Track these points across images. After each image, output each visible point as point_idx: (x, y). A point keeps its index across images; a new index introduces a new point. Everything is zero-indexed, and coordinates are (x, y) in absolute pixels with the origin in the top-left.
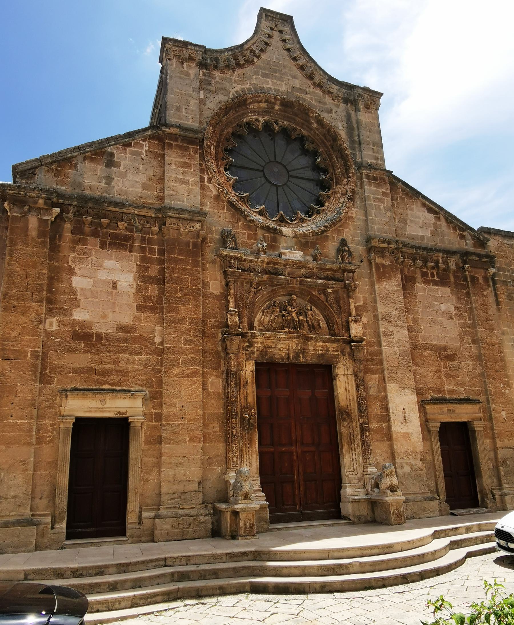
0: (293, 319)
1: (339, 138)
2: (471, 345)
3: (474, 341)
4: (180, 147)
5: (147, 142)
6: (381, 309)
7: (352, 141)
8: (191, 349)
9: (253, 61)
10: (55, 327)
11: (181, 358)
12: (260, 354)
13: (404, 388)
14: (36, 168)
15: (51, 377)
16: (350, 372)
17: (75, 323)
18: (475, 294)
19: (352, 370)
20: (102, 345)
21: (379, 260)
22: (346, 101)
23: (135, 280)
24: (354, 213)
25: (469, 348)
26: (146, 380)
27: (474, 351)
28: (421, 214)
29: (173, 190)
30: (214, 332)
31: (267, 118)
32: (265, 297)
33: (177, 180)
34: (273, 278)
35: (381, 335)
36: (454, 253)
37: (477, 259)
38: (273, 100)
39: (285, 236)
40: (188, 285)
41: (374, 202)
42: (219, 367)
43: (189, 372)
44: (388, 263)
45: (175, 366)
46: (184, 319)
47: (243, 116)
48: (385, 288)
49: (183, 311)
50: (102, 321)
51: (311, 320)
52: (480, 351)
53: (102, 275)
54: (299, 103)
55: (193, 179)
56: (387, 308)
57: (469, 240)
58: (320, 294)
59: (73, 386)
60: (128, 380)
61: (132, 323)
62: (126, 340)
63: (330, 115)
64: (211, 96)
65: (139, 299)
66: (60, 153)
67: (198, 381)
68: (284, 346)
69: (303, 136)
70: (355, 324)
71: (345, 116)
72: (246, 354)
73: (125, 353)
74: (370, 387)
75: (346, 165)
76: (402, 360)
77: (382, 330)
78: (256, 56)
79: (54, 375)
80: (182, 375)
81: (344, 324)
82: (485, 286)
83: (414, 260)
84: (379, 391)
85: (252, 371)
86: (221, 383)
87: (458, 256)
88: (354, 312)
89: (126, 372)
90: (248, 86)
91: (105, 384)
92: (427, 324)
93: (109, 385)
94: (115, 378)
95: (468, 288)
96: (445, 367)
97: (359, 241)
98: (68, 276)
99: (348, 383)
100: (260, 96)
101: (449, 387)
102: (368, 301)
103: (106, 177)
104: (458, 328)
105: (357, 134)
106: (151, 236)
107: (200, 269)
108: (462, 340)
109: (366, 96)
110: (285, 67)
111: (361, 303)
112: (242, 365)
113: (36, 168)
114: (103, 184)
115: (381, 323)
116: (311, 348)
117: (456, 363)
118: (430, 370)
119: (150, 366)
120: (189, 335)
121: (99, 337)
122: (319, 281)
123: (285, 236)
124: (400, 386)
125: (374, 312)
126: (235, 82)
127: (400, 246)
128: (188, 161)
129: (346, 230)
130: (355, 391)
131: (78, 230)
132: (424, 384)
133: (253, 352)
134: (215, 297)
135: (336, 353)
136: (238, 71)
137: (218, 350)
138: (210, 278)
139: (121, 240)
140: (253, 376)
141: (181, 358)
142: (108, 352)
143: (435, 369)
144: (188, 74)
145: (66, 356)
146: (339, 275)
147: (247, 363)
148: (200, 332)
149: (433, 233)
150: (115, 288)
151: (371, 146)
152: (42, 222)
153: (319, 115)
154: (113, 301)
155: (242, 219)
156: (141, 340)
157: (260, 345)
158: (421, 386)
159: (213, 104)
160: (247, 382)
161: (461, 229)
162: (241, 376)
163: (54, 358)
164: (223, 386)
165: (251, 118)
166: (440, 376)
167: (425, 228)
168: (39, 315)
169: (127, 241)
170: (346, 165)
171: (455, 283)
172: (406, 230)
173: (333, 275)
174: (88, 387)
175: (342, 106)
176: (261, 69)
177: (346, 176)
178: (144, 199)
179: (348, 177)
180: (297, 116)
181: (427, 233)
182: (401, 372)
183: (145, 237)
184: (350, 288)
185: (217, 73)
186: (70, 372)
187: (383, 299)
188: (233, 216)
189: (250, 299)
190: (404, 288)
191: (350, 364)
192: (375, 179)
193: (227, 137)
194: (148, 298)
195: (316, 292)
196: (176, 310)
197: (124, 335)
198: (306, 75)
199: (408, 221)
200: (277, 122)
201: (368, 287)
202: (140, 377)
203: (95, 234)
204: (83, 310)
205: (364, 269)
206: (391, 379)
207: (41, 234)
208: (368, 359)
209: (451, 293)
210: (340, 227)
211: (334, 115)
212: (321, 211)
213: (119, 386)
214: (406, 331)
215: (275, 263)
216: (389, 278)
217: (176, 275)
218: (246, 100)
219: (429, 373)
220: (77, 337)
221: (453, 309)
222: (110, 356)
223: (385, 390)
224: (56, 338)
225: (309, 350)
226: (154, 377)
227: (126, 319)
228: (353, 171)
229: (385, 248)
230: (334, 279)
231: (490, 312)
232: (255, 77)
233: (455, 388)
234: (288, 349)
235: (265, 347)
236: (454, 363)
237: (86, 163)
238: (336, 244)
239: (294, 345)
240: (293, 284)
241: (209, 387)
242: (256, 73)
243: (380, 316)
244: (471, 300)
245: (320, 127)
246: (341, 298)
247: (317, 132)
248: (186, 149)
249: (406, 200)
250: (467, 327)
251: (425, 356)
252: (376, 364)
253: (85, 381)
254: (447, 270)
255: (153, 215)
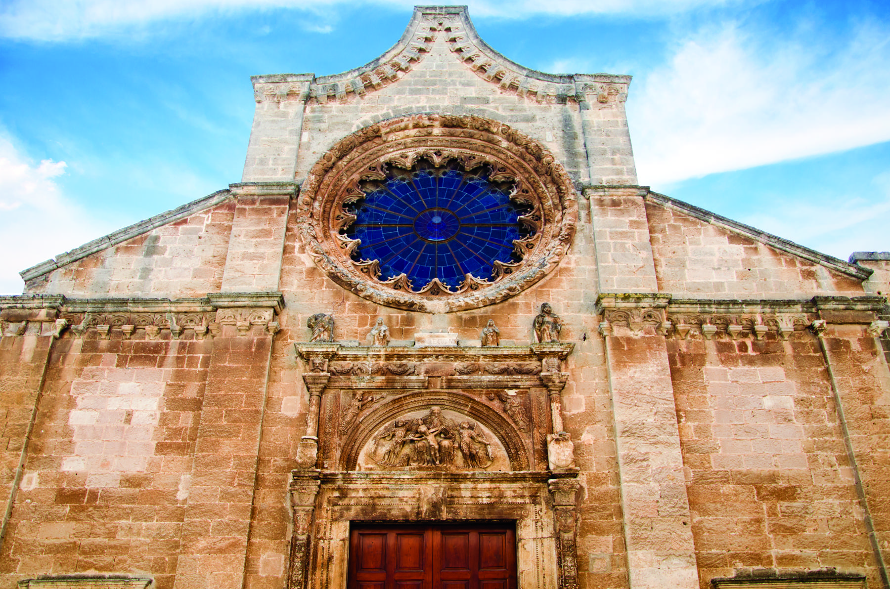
0: (430, 448)
1: (545, 153)
2: (836, 467)
3: (847, 459)
4: (257, 211)
5: (210, 214)
6: (621, 415)
7: (572, 153)
8: (232, 506)
9: (394, 77)
10: (35, 485)
11: (213, 523)
12: (362, 510)
13: (668, 556)
14: (50, 272)
15: (14, 560)
16: (547, 532)
17: (63, 476)
18: (841, 372)
19: (551, 528)
20: (96, 507)
21: (620, 332)
22: (563, 99)
23: (160, 407)
24: (573, 262)
25: (831, 473)
26: (155, 559)
27: (844, 476)
28: (715, 247)
29: (237, 271)
30: (280, 478)
31: (421, 150)
32: (381, 413)
33: (245, 256)
34: (394, 381)
35: (621, 461)
36: (789, 303)
37: (842, 307)
38: (427, 123)
39: (430, 313)
40: (241, 407)
41: (611, 238)
42: (284, 534)
43: (223, 544)
44: (640, 334)
45: (200, 535)
46: (226, 459)
47: (377, 155)
48: (632, 378)
49: (227, 447)
50: (102, 471)
51: (467, 445)
52: (857, 477)
53: (114, 404)
54: (473, 118)
55: (272, 249)
56: (636, 413)
57: (826, 278)
58: (491, 400)
59: (42, 573)
60: (125, 561)
61: (146, 472)
62: (133, 499)
63: (530, 124)
64: (320, 137)
65: (162, 434)
66: (82, 248)
67: (237, 558)
68: (410, 494)
69: (486, 164)
70: (556, 446)
71: (560, 121)
72: (333, 511)
73: (128, 519)
74: (594, 559)
75: (559, 190)
76: (666, 505)
77: (621, 452)
78: (401, 69)
79: (18, 557)
80: (212, 550)
81: (538, 447)
82: (866, 355)
83: (700, 324)
84: (613, 564)
85: (343, 540)
86: (283, 561)
87: (799, 307)
88: (558, 425)
89: (124, 549)
90: (384, 111)
91: (89, 568)
92: (729, 436)
93: (96, 569)
94: (107, 559)
95: (826, 362)
96: (772, 513)
97: (582, 305)
98: (66, 411)
99: (543, 553)
100: (402, 121)
101: (781, 551)
102: (597, 405)
103: (142, 269)
104: (805, 438)
105: (583, 142)
106: (195, 340)
107: (265, 380)
108: (813, 460)
109: (598, 85)
110: (450, 75)
111: (582, 409)
112: (322, 530)
113: (50, 272)
114: (137, 280)
115: (619, 440)
116: (466, 494)
117: (798, 504)
118: (735, 520)
119: (164, 537)
120: (231, 484)
121: (94, 495)
122: (487, 378)
123: (430, 313)
124: (659, 553)
125: (609, 422)
126: (363, 110)
127: (663, 302)
128: (267, 227)
129: (554, 290)
130: (555, 567)
131: (91, 347)
132: (719, 547)
133: (348, 507)
134: (289, 422)
135: (519, 501)
136: (371, 95)
137: (283, 507)
138: (284, 392)
139: (150, 351)
140: (344, 548)
141: (213, 523)
142: (103, 518)
143: (747, 518)
144: (285, 115)
145: (43, 527)
146: (533, 364)
147: (335, 526)
148: (250, 478)
149: (742, 277)
150: (128, 421)
151: (609, 156)
152: (42, 340)
153: (509, 128)
154: (123, 440)
155: (352, 296)
156: (157, 496)
157: (361, 494)
158: (713, 551)
159: (321, 145)
160: (330, 559)
161: (805, 261)
162: (320, 548)
163: (24, 531)
164: (286, 567)
165: (392, 154)
166: (758, 531)
167: (723, 269)
168: (11, 469)
169: (158, 352)
170: (559, 190)
171: (794, 357)
172: (683, 277)
173: (520, 365)
174: (64, 574)
175: (556, 108)
176: (410, 85)
177: (560, 208)
178: (193, 290)
179: (564, 208)
180: (472, 137)
181: (731, 277)
182: (663, 527)
183: (186, 344)
184: (550, 384)
185: (335, 105)
186: (42, 552)
187: (626, 397)
188: (337, 294)
189: (348, 419)
190: (675, 374)
191: (548, 518)
192: (615, 204)
193: (350, 186)
194: (177, 432)
195: (484, 397)
196: (215, 445)
197: (131, 491)
198: (489, 77)
199: (687, 263)
200: (438, 153)
201: (597, 380)
202: (146, 557)
203: (112, 349)
204: (77, 458)
205: (589, 352)
206: (637, 540)
207: (37, 356)
208: (594, 509)
209: (787, 375)
210: (542, 287)
211: (538, 124)
212: (513, 269)
213: (111, 571)
214: (677, 452)
215: (400, 357)
216: (644, 360)
217: (223, 393)
218: (379, 130)
219: (731, 526)
220: (63, 497)
221: (792, 404)
222: (104, 524)
223: (625, 562)
224: (33, 501)
225: (462, 497)
226: (168, 555)
227: (136, 466)
228: (572, 198)
229: (630, 309)
230: (520, 372)
231: (879, 402)
232: (397, 97)
233: (797, 552)
234: (419, 499)
235: (372, 498)
236: (794, 504)
237: (119, 256)
238: (534, 314)
239: (431, 490)
240: (435, 387)
241: (260, 570)
242: (399, 92)
243: (619, 428)
244: (832, 384)
245: (512, 144)
246: (534, 404)
247: (509, 153)
248: (266, 212)
249: (682, 228)
250: (826, 434)
251: (724, 495)
252: (611, 515)
253: (61, 565)
254: (774, 335)
255: (199, 309)
